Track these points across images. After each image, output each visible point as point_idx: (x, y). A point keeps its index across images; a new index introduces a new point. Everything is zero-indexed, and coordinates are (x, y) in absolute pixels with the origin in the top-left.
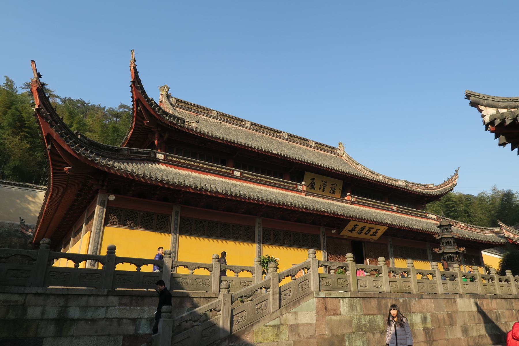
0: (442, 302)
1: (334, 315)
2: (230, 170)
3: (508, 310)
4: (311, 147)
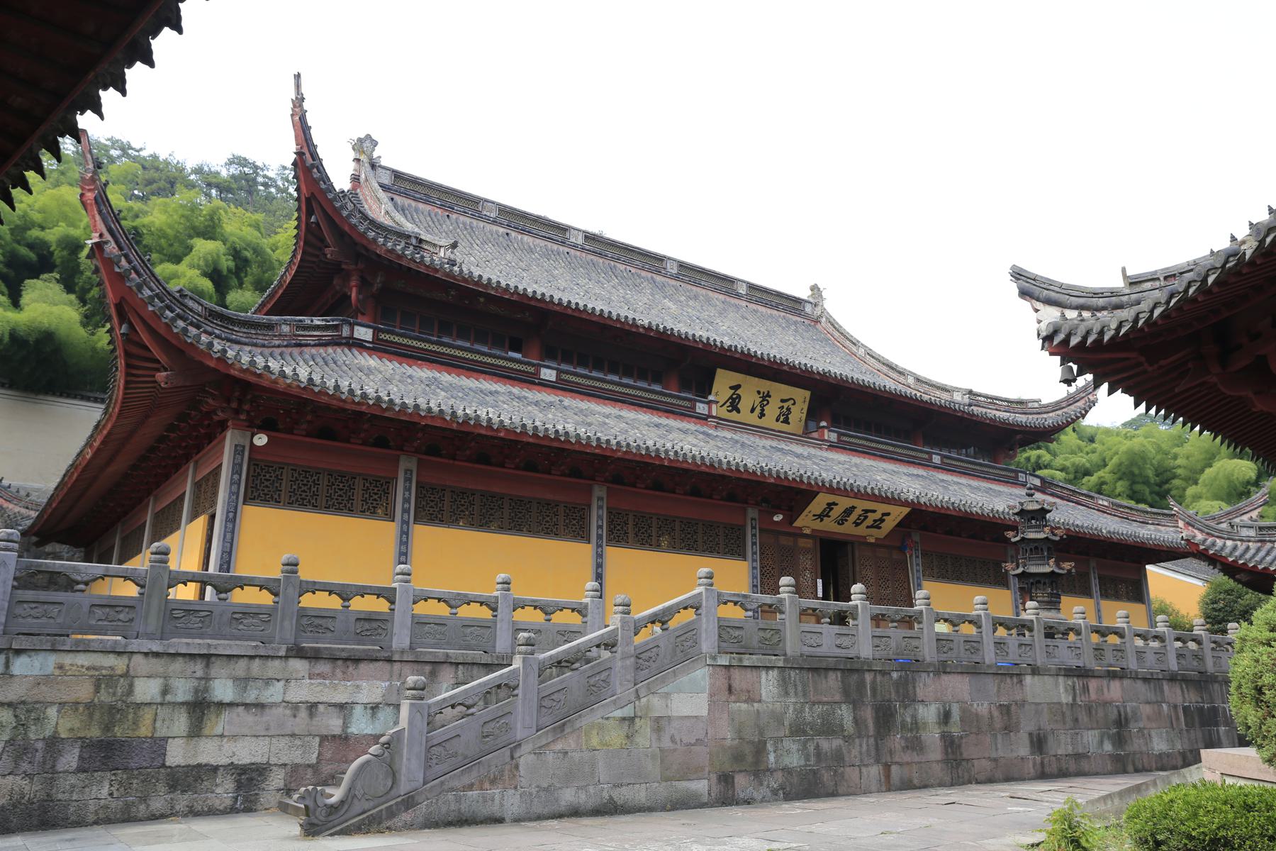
0: (991, 684)
1: (746, 701)
2: (533, 365)
3: (1148, 703)
4: (738, 296)
